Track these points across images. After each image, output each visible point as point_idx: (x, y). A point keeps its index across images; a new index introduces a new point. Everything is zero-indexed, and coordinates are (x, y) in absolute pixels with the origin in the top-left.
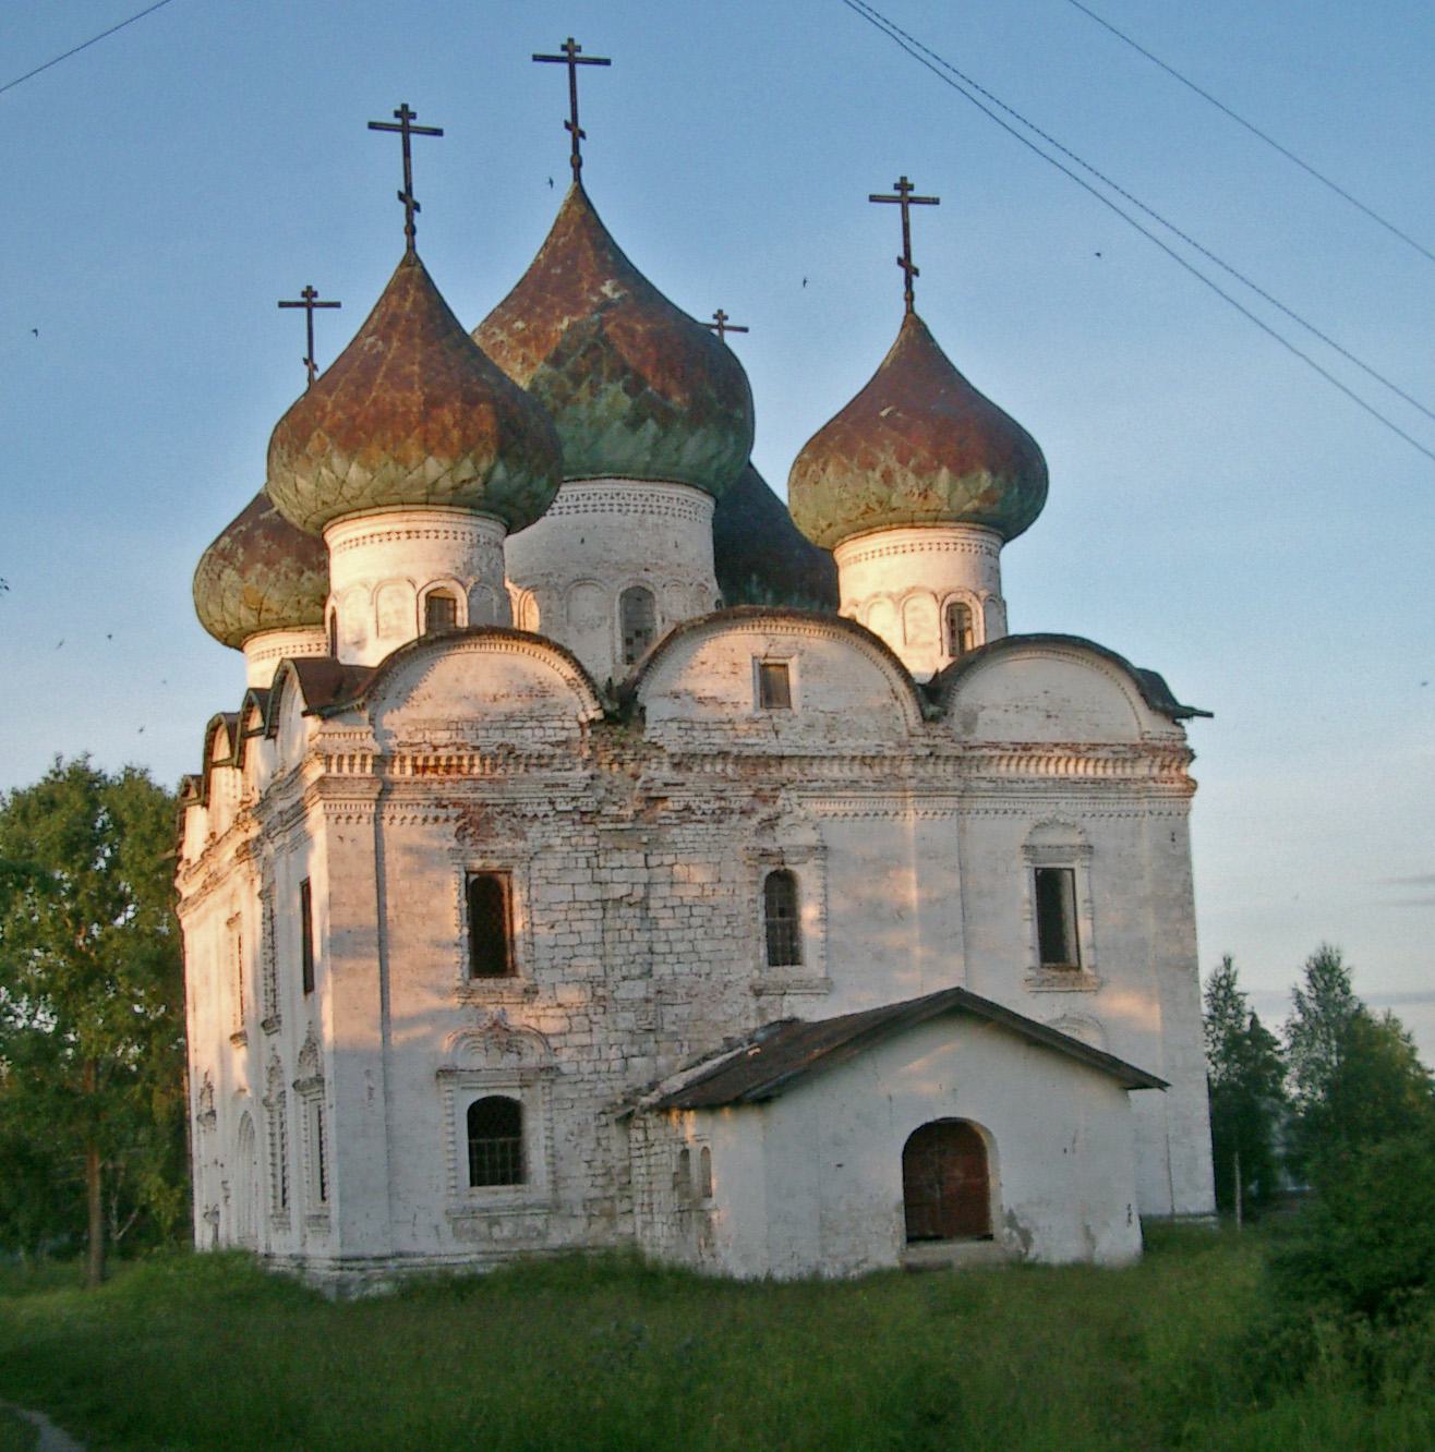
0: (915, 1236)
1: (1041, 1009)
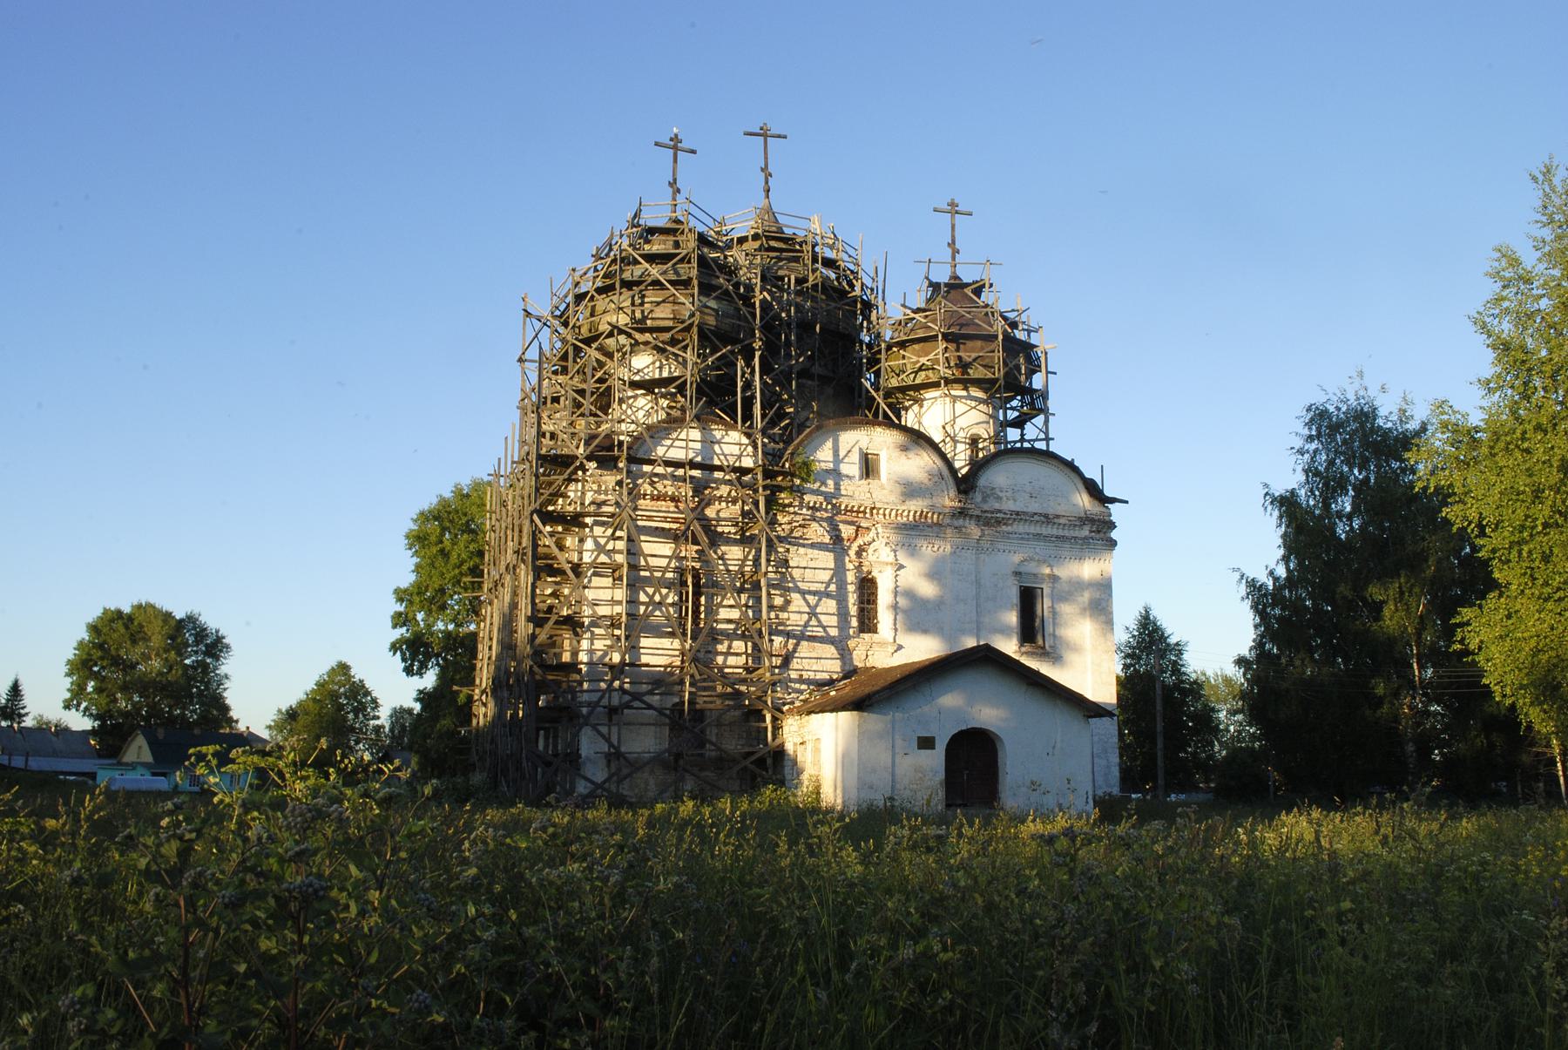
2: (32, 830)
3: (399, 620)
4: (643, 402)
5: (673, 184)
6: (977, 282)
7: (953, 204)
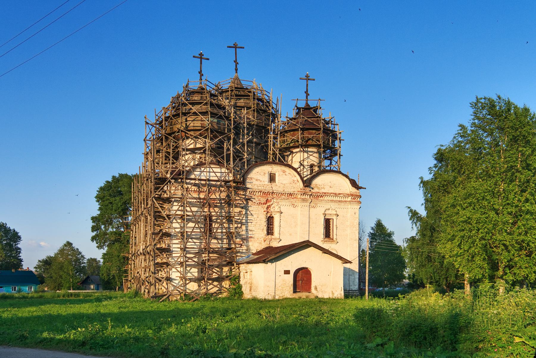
0: (295, 291)
1: (326, 246)
2: (208, 348)
3: (94, 229)
4: (189, 156)
5: (200, 72)
6: (315, 107)
7: (307, 76)
